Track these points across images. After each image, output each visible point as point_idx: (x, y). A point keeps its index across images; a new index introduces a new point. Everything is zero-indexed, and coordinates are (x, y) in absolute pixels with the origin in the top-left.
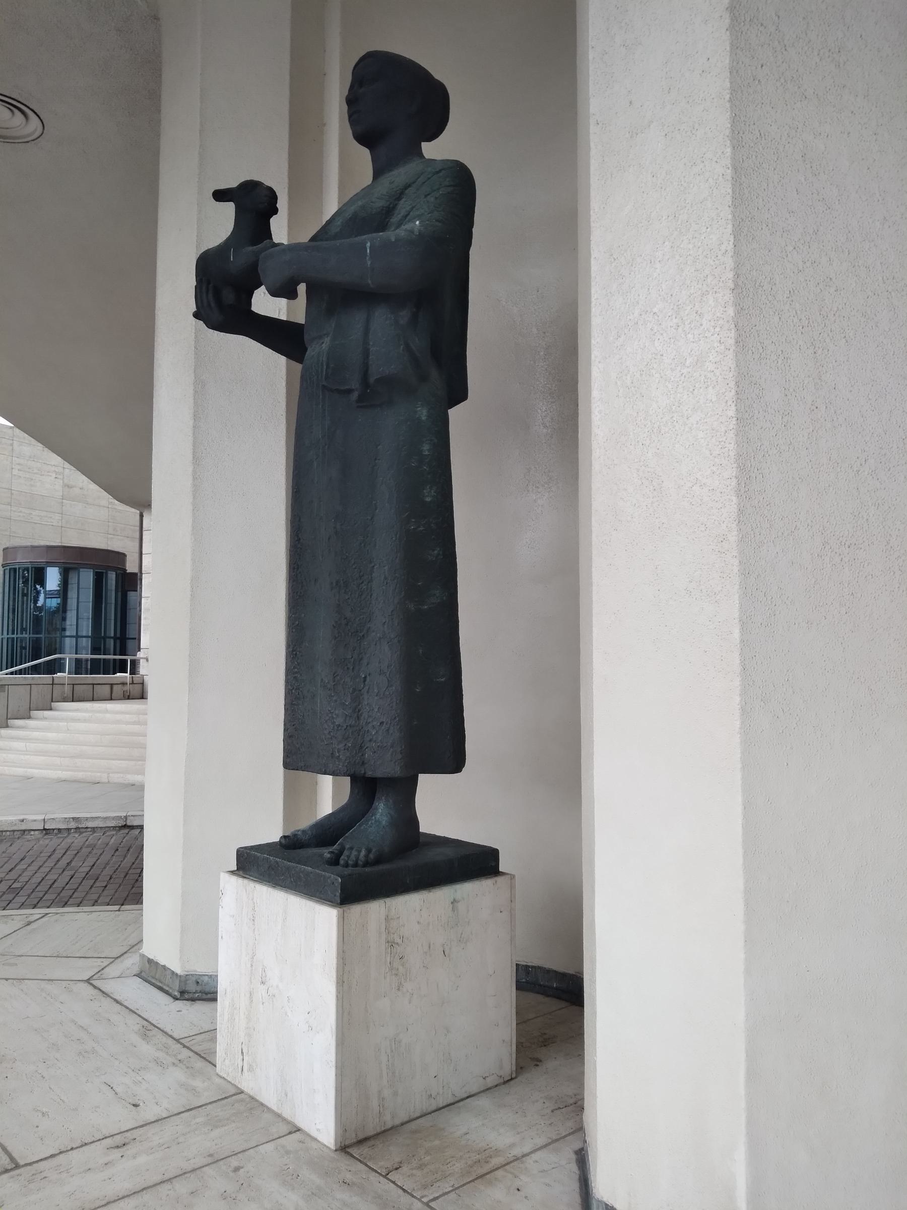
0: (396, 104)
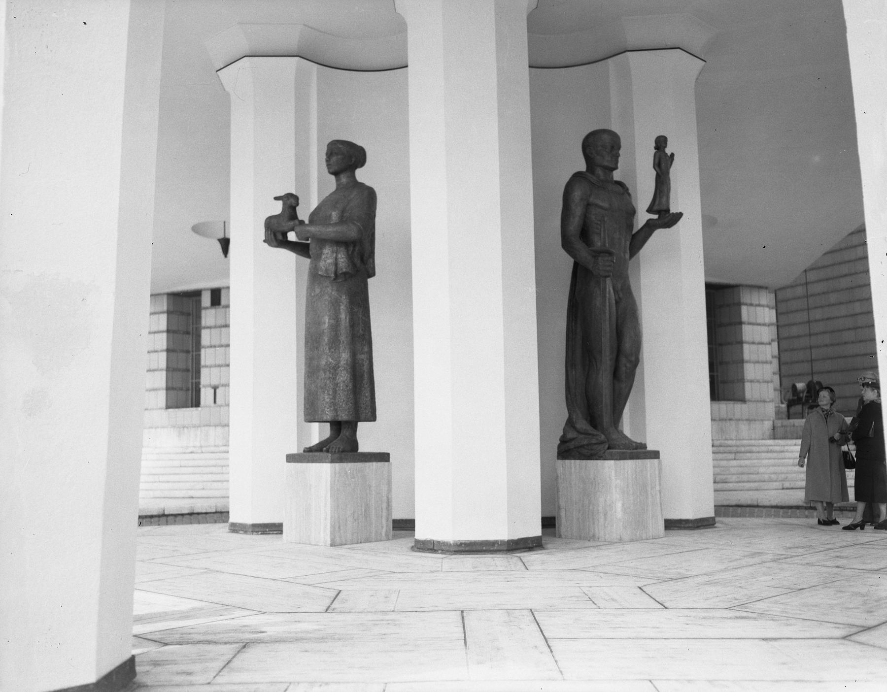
0: (346, 158)
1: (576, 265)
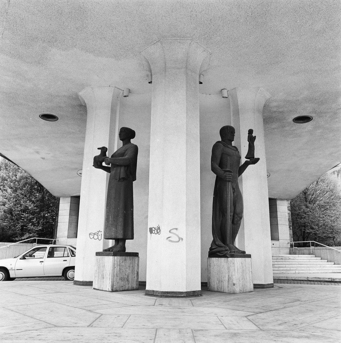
0: (127, 134)
1: (217, 177)
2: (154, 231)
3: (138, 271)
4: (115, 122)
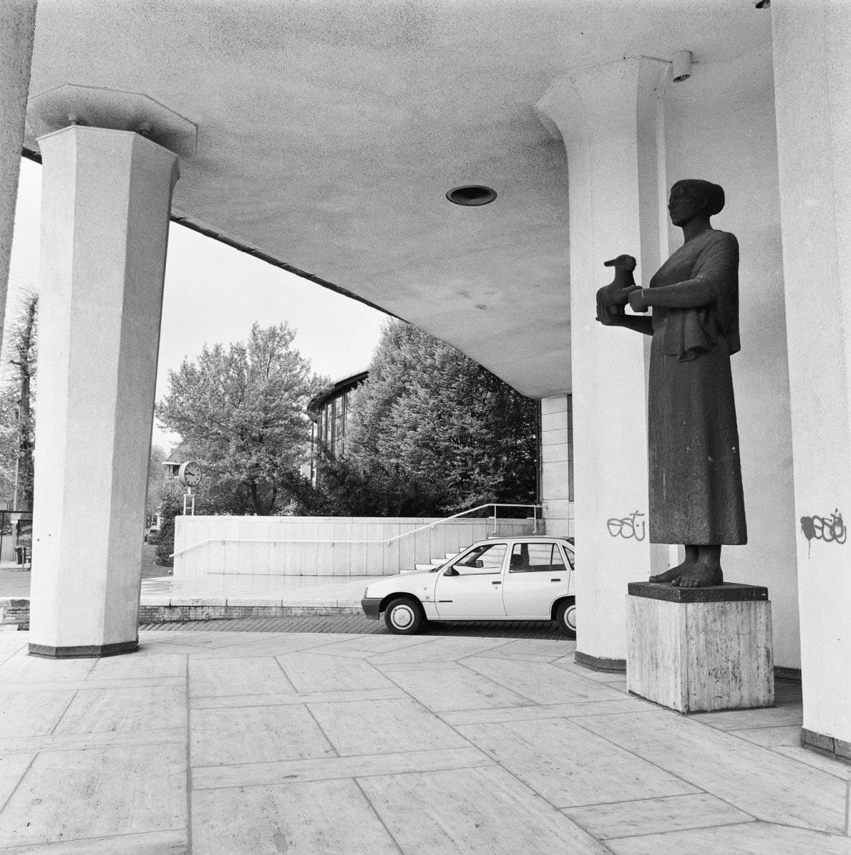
0: (696, 202)
2: (822, 529)
3: (769, 647)
4: (655, 168)
